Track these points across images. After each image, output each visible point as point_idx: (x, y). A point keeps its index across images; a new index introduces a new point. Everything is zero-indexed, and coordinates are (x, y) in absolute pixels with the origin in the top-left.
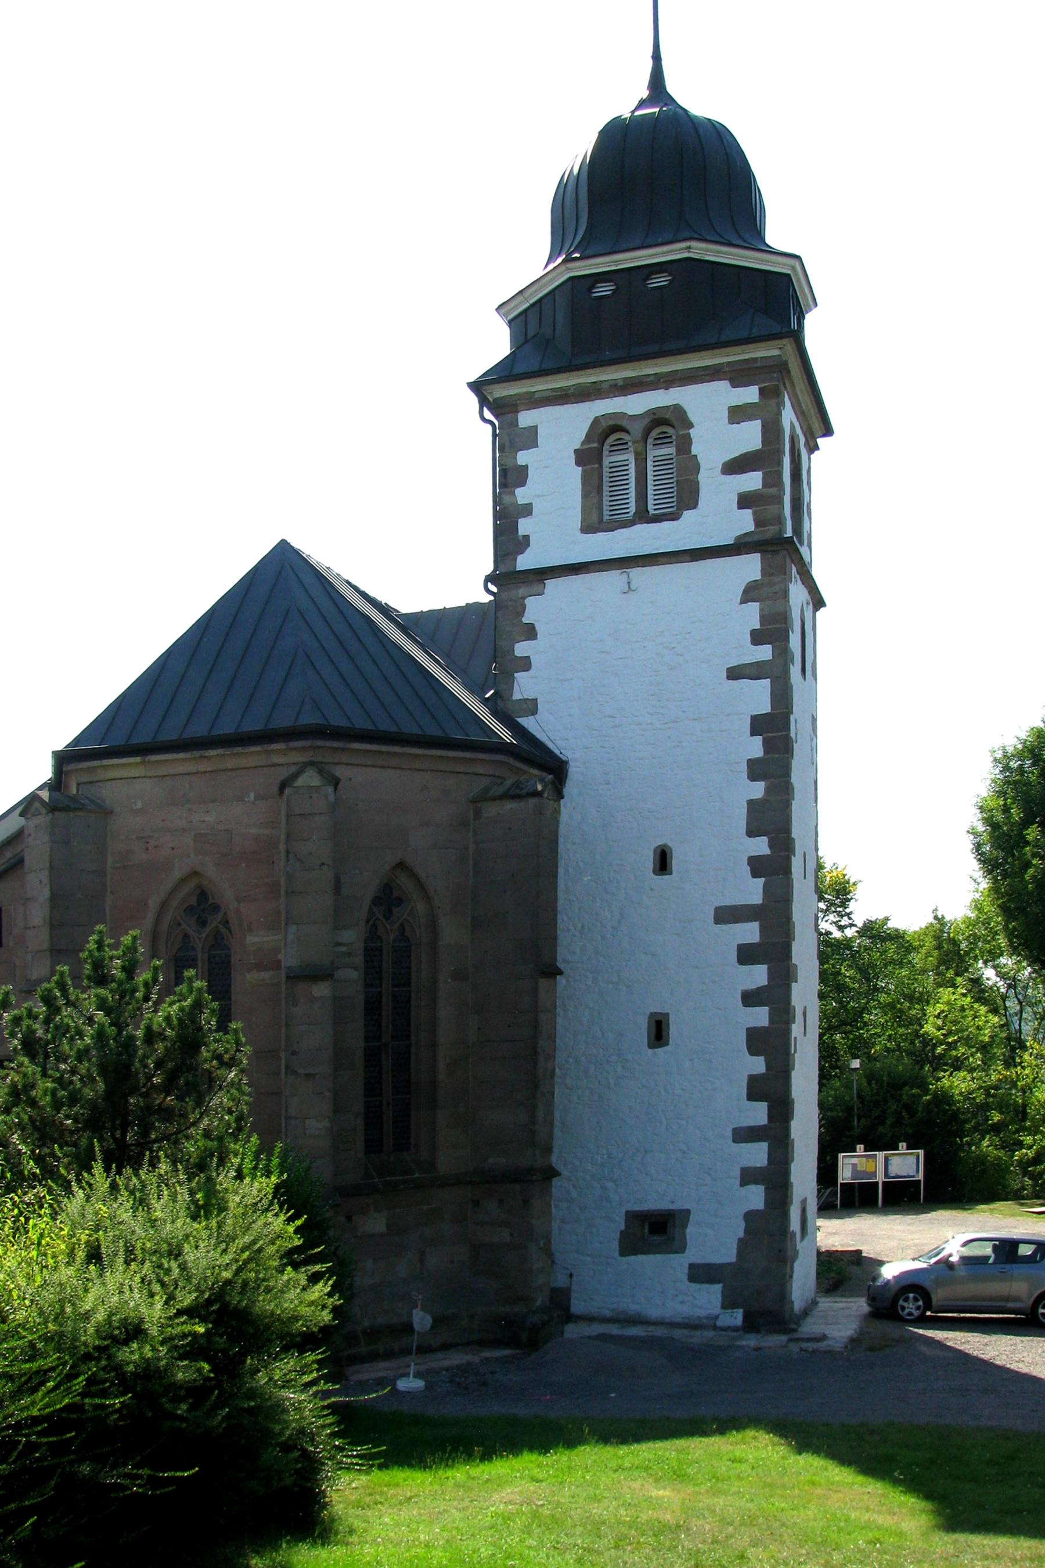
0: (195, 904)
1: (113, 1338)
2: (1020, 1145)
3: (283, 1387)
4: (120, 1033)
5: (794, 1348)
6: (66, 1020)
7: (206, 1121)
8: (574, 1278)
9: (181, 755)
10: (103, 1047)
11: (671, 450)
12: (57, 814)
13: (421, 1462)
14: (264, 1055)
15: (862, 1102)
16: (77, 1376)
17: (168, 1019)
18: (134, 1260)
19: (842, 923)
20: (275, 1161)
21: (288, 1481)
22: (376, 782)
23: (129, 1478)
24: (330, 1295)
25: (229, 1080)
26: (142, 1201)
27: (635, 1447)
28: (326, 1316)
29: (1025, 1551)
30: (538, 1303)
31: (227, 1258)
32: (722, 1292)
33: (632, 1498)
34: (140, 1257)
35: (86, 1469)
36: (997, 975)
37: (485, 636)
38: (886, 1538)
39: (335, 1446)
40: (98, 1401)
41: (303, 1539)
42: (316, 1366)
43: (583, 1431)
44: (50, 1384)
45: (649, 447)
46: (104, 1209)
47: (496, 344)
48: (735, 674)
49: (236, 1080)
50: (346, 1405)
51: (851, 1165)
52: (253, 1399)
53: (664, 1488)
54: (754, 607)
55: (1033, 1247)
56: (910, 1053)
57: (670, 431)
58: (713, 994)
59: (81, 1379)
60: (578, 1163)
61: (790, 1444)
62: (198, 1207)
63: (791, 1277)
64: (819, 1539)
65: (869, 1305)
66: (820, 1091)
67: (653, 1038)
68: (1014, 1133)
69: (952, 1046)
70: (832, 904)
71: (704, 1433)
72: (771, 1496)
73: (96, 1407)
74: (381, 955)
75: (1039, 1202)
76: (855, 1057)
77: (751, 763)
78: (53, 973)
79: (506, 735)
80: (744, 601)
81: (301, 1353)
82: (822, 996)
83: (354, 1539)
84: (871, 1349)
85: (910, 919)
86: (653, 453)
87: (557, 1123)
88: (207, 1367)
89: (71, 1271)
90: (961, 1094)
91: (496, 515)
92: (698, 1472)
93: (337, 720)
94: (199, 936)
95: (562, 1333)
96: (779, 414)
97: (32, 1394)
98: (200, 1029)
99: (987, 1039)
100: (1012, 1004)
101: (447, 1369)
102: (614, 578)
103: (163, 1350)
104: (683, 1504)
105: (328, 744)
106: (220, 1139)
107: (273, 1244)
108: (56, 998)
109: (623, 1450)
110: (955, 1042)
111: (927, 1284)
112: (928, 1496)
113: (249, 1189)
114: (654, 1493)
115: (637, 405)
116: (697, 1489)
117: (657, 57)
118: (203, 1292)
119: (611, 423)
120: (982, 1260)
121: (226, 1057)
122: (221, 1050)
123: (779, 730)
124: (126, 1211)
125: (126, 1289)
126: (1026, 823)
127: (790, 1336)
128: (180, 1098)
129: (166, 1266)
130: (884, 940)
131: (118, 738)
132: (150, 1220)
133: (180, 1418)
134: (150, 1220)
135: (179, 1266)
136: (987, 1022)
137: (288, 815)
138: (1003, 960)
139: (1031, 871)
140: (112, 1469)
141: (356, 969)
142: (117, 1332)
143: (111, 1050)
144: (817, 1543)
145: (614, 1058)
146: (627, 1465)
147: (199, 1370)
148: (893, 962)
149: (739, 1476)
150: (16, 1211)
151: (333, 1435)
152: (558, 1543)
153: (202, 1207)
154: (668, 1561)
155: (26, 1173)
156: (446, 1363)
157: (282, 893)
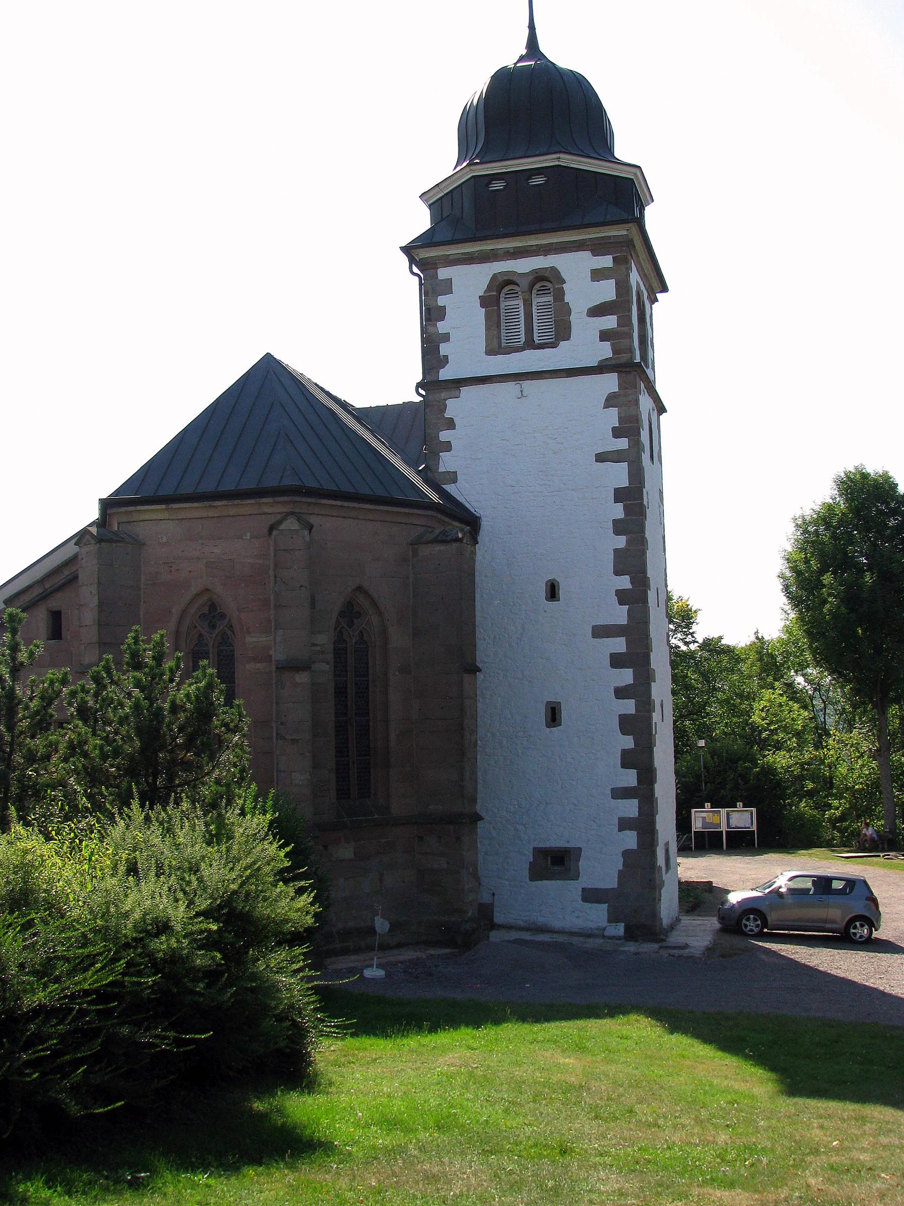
1: (147, 932)
2: (830, 806)
3: (277, 972)
4: (151, 705)
5: (664, 953)
6: (110, 695)
7: (217, 772)
8: (496, 896)
9: (196, 505)
10: (139, 715)
12: (103, 544)
13: (383, 1032)
15: (708, 772)
16: (119, 960)
17: (188, 696)
18: (163, 874)
19: (687, 640)
20: (270, 803)
21: (282, 1044)
22: (338, 527)
23: (158, 1038)
24: (312, 904)
26: (168, 830)
27: (546, 1025)
28: (309, 920)
30: (469, 914)
31: (234, 875)
33: (545, 1064)
35: (125, 1030)
36: (805, 681)
37: (417, 426)
41: (293, 1089)
43: (506, 1013)
44: (98, 965)
47: (421, 221)
48: (601, 458)
50: (326, 987)
51: (700, 818)
52: (252, 981)
53: (570, 1057)
54: (614, 412)
55: (843, 883)
56: (741, 737)
57: (549, 285)
59: (122, 962)
61: (664, 1027)
65: (720, 923)
68: (824, 798)
70: (679, 626)
71: (598, 1016)
72: (652, 1065)
77: (615, 522)
78: (101, 660)
79: (434, 497)
80: (606, 406)
82: (674, 693)
83: (333, 1089)
84: (723, 956)
85: (738, 638)
87: (480, 781)
89: (114, 881)
92: (595, 1045)
93: (311, 483)
94: (210, 635)
98: (212, 704)
100: (818, 703)
101: (402, 963)
103: (185, 942)
104: (584, 1069)
105: (304, 499)
106: (228, 785)
108: (103, 678)
109: (537, 1027)
110: (776, 729)
111: (763, 909)
112: (773, 1069)
113: (250, 824)
115: (524, 266)
117: (532, 27)
118: (216, 899)
119: (505, 278)
120: (804, 892)
121: (232, 725)
123: (635, 499)
124: (157, 837)
125: (157, 895)
126: (822, 571)
128: (197, 754)
129: (187, 879)
130: (719, 653)
131: (148, 491)
132: (175, 844)
133: (199, 994)
134: (175, 844)
135: (197, 879)
137: (275, 550)
138: (809, 670)
139: (828, 606)
140: (145, 1031)
141: (328, 663)
142: (150, 927)
147: (213, 958)
148: (726, 669)
150: (72, 835)
151: (316, 1010)
152: (489, 1096)
156: (401, 958)
157: (272, 603)
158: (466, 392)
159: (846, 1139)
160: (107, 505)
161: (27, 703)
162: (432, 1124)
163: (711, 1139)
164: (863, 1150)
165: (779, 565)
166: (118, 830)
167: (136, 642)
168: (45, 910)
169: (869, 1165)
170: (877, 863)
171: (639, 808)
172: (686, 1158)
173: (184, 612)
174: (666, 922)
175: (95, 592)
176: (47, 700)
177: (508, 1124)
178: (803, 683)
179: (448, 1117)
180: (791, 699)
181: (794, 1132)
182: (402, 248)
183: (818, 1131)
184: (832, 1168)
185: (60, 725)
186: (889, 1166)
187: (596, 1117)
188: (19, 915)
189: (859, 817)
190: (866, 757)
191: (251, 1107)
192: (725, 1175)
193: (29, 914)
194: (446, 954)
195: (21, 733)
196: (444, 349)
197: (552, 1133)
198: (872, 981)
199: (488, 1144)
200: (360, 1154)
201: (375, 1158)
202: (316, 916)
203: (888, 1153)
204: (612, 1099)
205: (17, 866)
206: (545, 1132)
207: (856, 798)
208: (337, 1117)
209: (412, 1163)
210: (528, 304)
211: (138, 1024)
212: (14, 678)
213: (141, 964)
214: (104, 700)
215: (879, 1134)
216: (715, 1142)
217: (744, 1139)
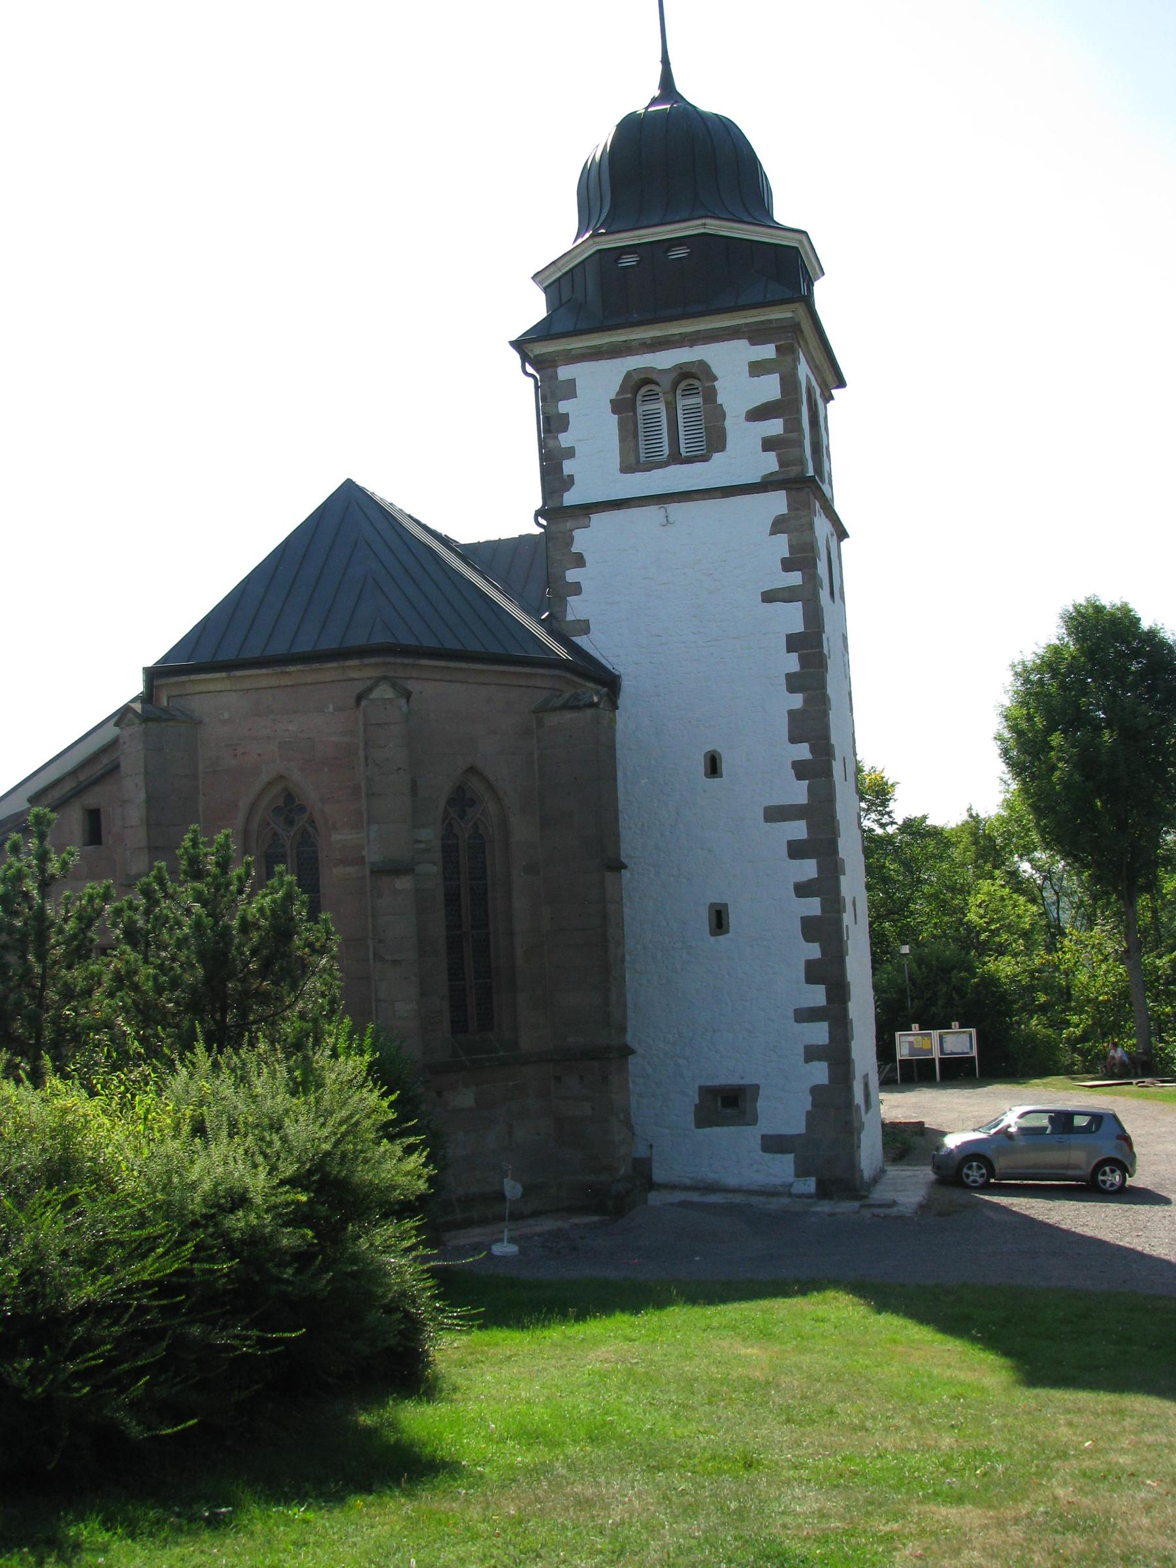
1: (220, 1207)
2: (1068, 1024)
3: (384, 1252)
4: (216, 923)
5: (867, 1213)
6: (165, 912)
7: (301, 1004)
8: (654, 1149)
9: (264, 671)
10: (201, 936)
12: (150, 724)
13: (519, 1322)
15: (914, 985)
16: (185, 1243)
17: (261, 910)
18: (237, 1133)
19: (884, 821)
20: (368, 1041)
21: (392, 1341)
22: (443, 694)
23: (238, 1338)
24: (425, 1165)
28: (422, 1185)
30: (622, 1172)
31: (325, 1132)
34: (243, 1130)
35: (196, 1330)
36: (1032, 868)
37: (538, 564)
39: (436, 1308)
40: (207, 1266)
41: (409, 1397)
42: (414, 1232)
43: (671, 1293)
44: (160, 1250)
45: (678, 397)
47: (533, 308)
48: (769, 597)
49: (328, 966)
50: (446, 1269)
51: (907, 1043)
53: (752, 1346)
54: (783, 540)
55: (1088, 1118)
56: (955, 940)
57: (697, 383)
58: (767, 887)
59: (189, 1245)
61: (869, 1305)
62: (297, 1084)
63: (859, 1147)
64: (904, 1395)
65: (935, 1173)
66: (873, 975)
67: (714, 926)
71: (786, 1294)
72: (855, 1354)
73: (204, 1271)
75: (1090, 1076)
77: (789, 676)
78: (151, 868)
79: (562, 652)
80: (773, 533)
81: (400, 1220)
82: (869, 887)
83: (458, 1396)
84: (940, 1214)
85: (946, 815)
86: (681, 403)
87: (629, 1005)
89: (177, 1144)
90: (1007, 976)
91: (543, 458)
93: (407, 640)
94: (287, 834)
97: (142, 1259)
98: (292, 919)
99: (1027, 926)
100: (1049, 895)
101: (539, 1235)
102: (653, 513)
103: (268, 1217)
105: (399, 660)
106: (315, 1020)
108: (155, 891)
109: (710, 1311)
110: (998, 929)
111: (989, 1153)
112: (1007, 1353)
113: (344, 1067)
114: (743, 1351)
115: (665, 360)
116: (783, 1347)
117: (665, 61)
118: (304, 1163)
119: (642, 376)
120: (1040, 1131)
121: (318, 945)
122: (312, 938)
126: (1049, 730)
128: (276, 983)
130: (923, 836)
131: (204, 656)
132: (251, 1096)
133: (288, 1282)
134: (251, 1096)
135: (281, 1139)
136: (1026, 910)
138: (1037, 854)
139: (1057, 773)
140: (221, 1330)
141: (435, 864)
142: (223, 1201)
143: (208, 939)
146: (715, 1324)
147: (303, 1236)
148: (933, 856)
150: (122, 1088)
151: (434, 1297)
153: (301, 1083)
154: (761, 1416)
156: (538, 1229)
157: (363, 795)
159: (1102, 1438)
160: (153, 675)
162: (583, 1435)
163: (933, 1443)
164: (1123, 1451)
165: (995, 725)
168: (92, 1183)
169: (1131, 1470)
171: (830, 1033)
172: (902, 1469)
173: (253, 806)
176: (86, 920)
177: (679, 1432)
178: (1030, 870)
179: (603, 1426)
180: (1015, 891)
183: (1064, 1430)
184: (1084, 1475)
185: (103, 951)
186: (1156, 1471)
187: (788, 1421)
189: (1104, 1035)
190: (1111, 961)
192: (951, 1488)
195: (55, 963)
196: (568, 467)
197: (733, 1442)
198: (1127, 1239)
199: (654, 1458)
200: (495, 1476)
201: (514, 1480)
203: (1154, 1454)
204: (806, 1398)
205: (55, 1130)
206: (725, 1441)
207: (1100, 1012)
208: (465, 1430)
209: (560, 1486)
212: (44, 894)
213: (214, 1246)
214: (157, 918)
215: (1143, 1431)
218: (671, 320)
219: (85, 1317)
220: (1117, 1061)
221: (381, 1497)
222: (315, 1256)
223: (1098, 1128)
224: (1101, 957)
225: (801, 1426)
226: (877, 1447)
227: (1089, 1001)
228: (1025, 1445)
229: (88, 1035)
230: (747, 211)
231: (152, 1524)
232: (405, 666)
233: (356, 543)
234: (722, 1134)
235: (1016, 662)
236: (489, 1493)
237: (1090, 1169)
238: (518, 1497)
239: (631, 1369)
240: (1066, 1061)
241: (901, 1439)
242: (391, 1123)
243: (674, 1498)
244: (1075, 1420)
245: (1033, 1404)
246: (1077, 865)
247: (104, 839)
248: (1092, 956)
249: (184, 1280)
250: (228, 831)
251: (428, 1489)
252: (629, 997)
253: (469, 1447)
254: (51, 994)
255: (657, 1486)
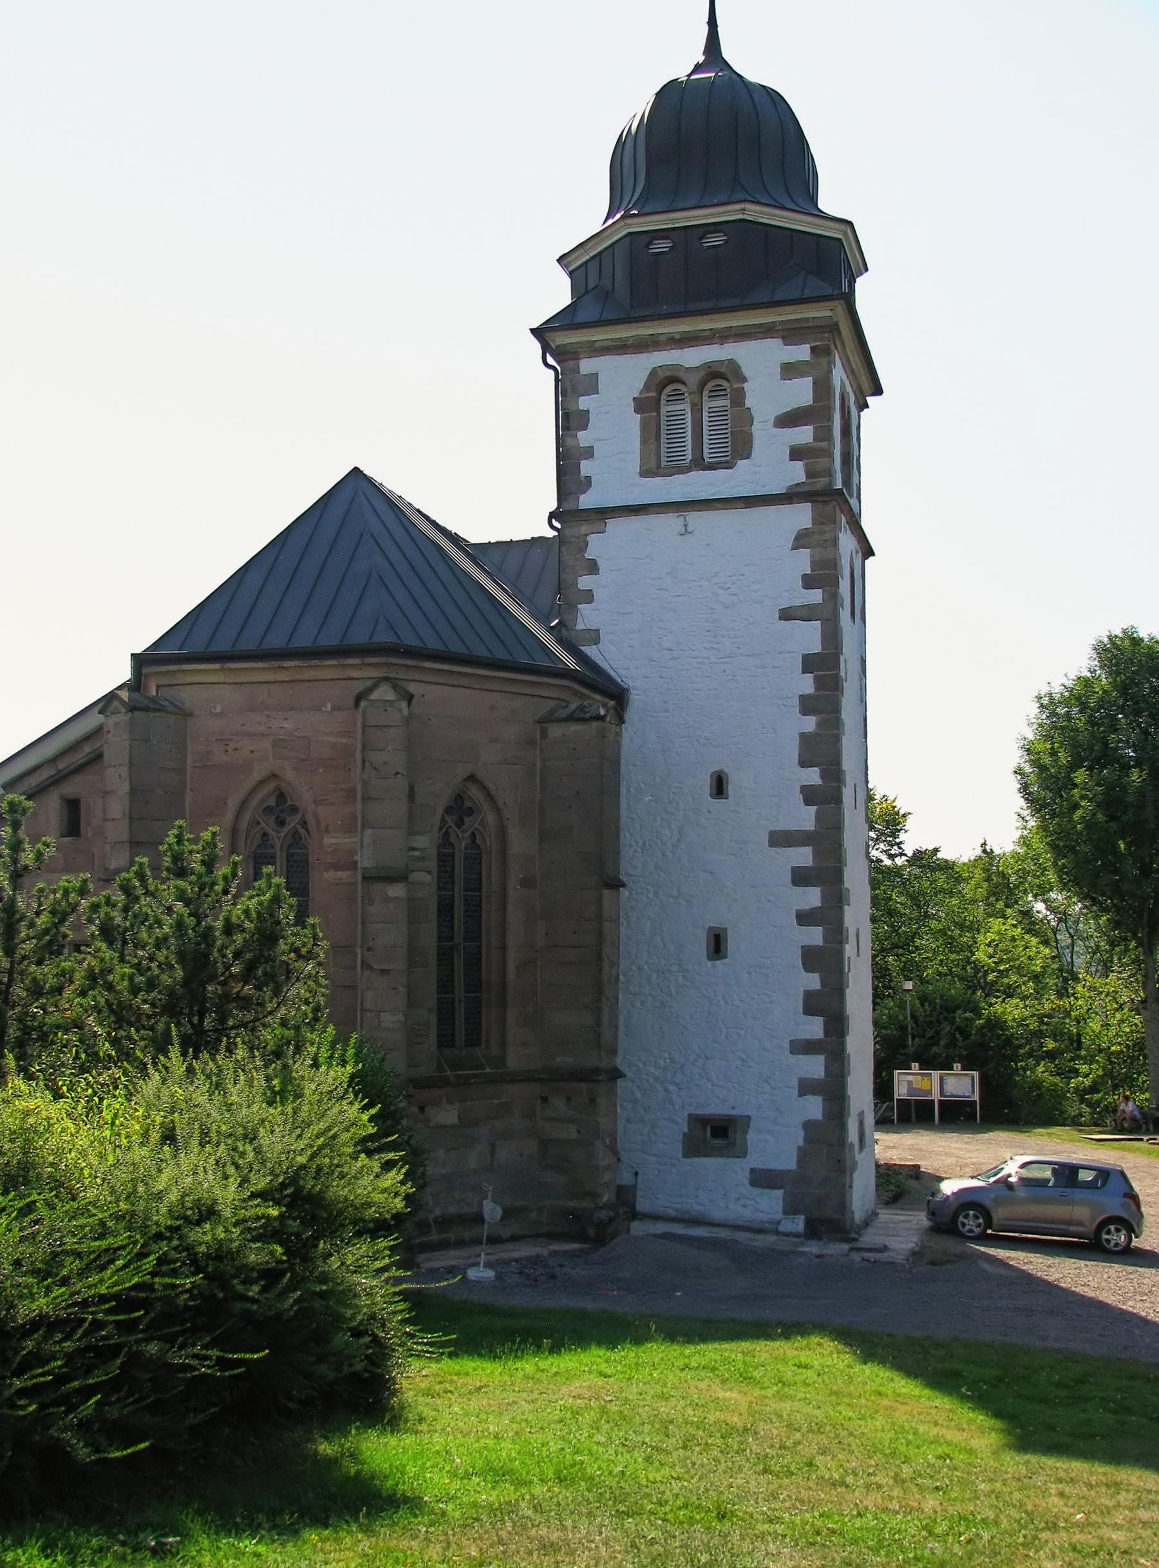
0: (274, 804)
1: (186, 1218)
2: (1076, 1072)
3: (355, 1272)
4: (199, 923)
5: (856, 1257)
6: (144, 909)
7: (283, 1011)
8: (639, 1177)
9: (260, 665)
10: (182, 936)
11: (726, 402)
12: (137, 713)
13: (491, 1351)
14: (341, 950)
15: (916, 1022)
16: (147, 1255)
17: (247, 912)
18: (209, 1142)
19: (893, 852)
20: (351, 1052)
21: (359, 1367)
22: (445, 698)
23: (198, 1358)
24: (403, 1183)
25: (306, 972)
26: (217, 1085)
27: (702, 1347)
28: (399, 1204)
29: (1100, 1477)
30: (605, 1199)
31: (302, 1144)
32: (784, 1198)
33: (699, 1398)
34: (215, 1139)
35: (153, 1348)
36: (1047, 909)
37: (549, 567)
38: (956, 1454)
39: (406, 1333)
40: (168, 1280)
41: (372, 1426)
42: (387, 1252)
43: (650, 1328)
44: (120, 1263)
45: (705, 398)
46: (180, 1091)
47: (557, 293)
48: (786, 615)
49: (314, 973)
50: (418, 1292)
51: (908, 1082)
52: (323, 1282)
53: (731, 1390)
54: (805, 555)
55: (1094, 1173)
56: (961, 979)
57: (725, 384)
58: (770, 916)
59: (151, 1258)
60: (641, 1066)
61: (855, 1353)
62: (275, 1093)
63: (851, 1187)
64: (888, 1451)
65: (929, 1219)
66: (874, 1009)
67: (712, 951)
68: (1070, 1061)
69: (1003, 974)
70: (882, 834)
71: (769, 1337)
72: (838, 1404)
73: (166, 1286)
74: (453, 861)
75: (1098, 1129)
76: (908, 979)
77: (803, 698)
78: (132, 864)
79: (571, 663)
80: (795, 548)
81: (373, 1239)
82: (874, 920)
83: (424, 1427)
84: (933, 1263)
85: (959, 849)
86: (708, 404)
87: (621, 1027)
88: (280, 1250)
89: (144, 1151)
90: (1014, 1020)
91: (559, 456)
92: (764, 1376)
93: (411, 641)
94: (278, 834)
95: (629, 1230)
96: (830, 372)
97: (100, 1272)
98: (278, 923)
99: (1039, 969)
100: (1063, 938)
101: (516, 1261)
102: (670, 522)
103: (236, 1231)
104: (750, 1407)
105: (401, 661)
106: (297, 1028)
107: (348, 1131)
108: (135, 887)
109: (689, 1350)
110: (1007, 970)
111: (987, 1202)
112: (998, 1415)
113: (325, 1077)
114: (721, 1394)
115: (693, 357)
116: (763, 1392)
118: (277, 1176)
119: (668, 374)
120: (1041, 1183)
121: (304, 950)
122: (298, 944)
123: (829, 669)
124: (202, 1094)
125: (200, 1170)
126: (1074, 766)
127: (851, 1245)
128: (258, 988)
129: (241, 1149)
130: (933, 870)
131: (198, 644)
132: (226, 1104)
133: (253, 1301)
134: (226, 1104)
135: (254, 1149)
136: (1038, 952)
137: (364, 726)
138: (1053, 895)
139: (1079, 812)
140: (181, 1348)
141: (429, 872)
142: (189, 1213)
143: (190, 939)
144: (885, 1455)
145: (674, 968)
146: (694, 1364)
147: (272, 1253)
148: (943, 891)
149: (805, 1382)
150: (90, 1091)
151: (404, 1322)
152: (626, 1440)
153: (278, 1093)
154: (736, 1465)
155: (101, 1054)
156: (516, 1255)
157: (359, 798)
158: (613, 525)
159: (1094, 1511)
160: (138, 660)
161: (32, 919)
162: (551, 1475)
163: (916, 1504)
164: (1117, 1527)
165: (1016, 757)
166: (150, 1086)
167: (180, 842)
168: (51, 1190)
169: (1124, 1547)
170: (1138, 1149)
171: (826, 1067)
172: (882, 1530)
173: (243, 805)
174: (858, 1216)
175: (125, 775)
176: (60, 915)
177: (651, 1477)
178: (1044, 911)
179: (572, 1466)
180: (1028, 932)
181: (1025, 1500)
182: (533, 331)
183: (1056, 1500)
184: (1074, 1549)
185: (77, 948)
186: (1151, 1550)
187: (765, 1471)
188: (15, 1196)
189: (1115, 1087)
190: (1126, 1010)
191: (316, 1450)
192: (933, 1553)
193: (30, 1195)
194: (574, 1250)
195: (24, 958)
196: (586, 467)
197: (707, 1490)
198: (1130, 1303)
199: (623, 1503)
200: (457, 1514)
201: (477, 1520)
202: (408, 1198)
203: (1149, 1532)
204: (785, 1448)
205: (15, 1132)
206: (698, 1488)
207: (1111, 1063)
208: (428, 1464)
209: (524, 1528)
210: (697, 409)
211: (170, 1340)
212: (15, 887)
213: (176, 1261)
214: (135, 916)
215: (1138, 1507)
216: (920, 1509)
217: (958, 1507)
218: (702, 314)
219: (37, 1330)
220: (1127, 1116)
221: (337, 1532)
222: (282, 1274)
223: (1104, 1184)
224: (1115, 1006)
225: (778, 1477)
226: (857, 1505)
227: (1100, 1051)
228: (1014, 1513)
229: (56, 1034)
230: (793, 201)
231: (94, 1552)
232: (409, 667)
233: (362, 536)
234: (710, 1164)
235: (1043, 694)
236: (450, 1532)
237: (1095, 1225)
238: (481, 1538)
239: (605, 1407)
240: (1073, 1112)
241: (883, 1498)
242: (371, 1138)
243: (643, 1547)
244: (1067, 1490)
245: (1023, 1470)
246: (1095, 908)
247: (82, 832)
248: (1105, 1005)
249: (144, 1295)
250: (216, 829)
251: (387, 1525)
252: (621, 1019)
253: (433, 1483)
254: (18, 990)
255: (626, 1532)
